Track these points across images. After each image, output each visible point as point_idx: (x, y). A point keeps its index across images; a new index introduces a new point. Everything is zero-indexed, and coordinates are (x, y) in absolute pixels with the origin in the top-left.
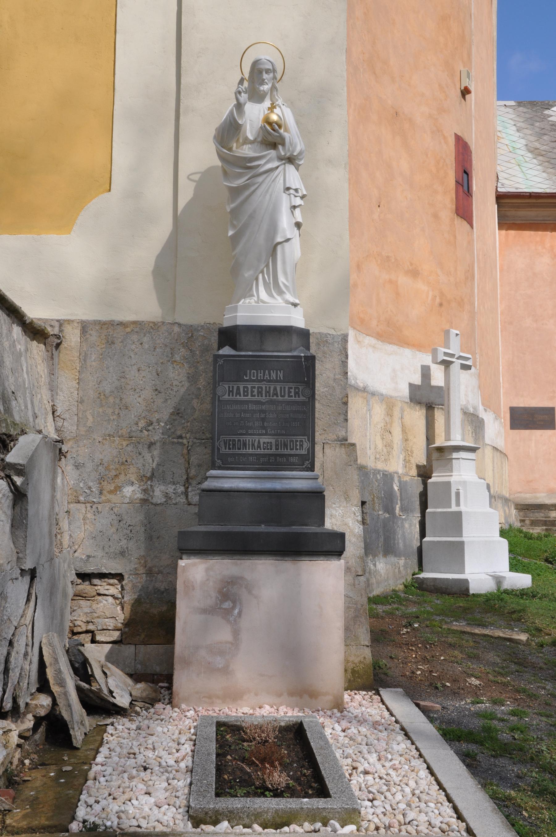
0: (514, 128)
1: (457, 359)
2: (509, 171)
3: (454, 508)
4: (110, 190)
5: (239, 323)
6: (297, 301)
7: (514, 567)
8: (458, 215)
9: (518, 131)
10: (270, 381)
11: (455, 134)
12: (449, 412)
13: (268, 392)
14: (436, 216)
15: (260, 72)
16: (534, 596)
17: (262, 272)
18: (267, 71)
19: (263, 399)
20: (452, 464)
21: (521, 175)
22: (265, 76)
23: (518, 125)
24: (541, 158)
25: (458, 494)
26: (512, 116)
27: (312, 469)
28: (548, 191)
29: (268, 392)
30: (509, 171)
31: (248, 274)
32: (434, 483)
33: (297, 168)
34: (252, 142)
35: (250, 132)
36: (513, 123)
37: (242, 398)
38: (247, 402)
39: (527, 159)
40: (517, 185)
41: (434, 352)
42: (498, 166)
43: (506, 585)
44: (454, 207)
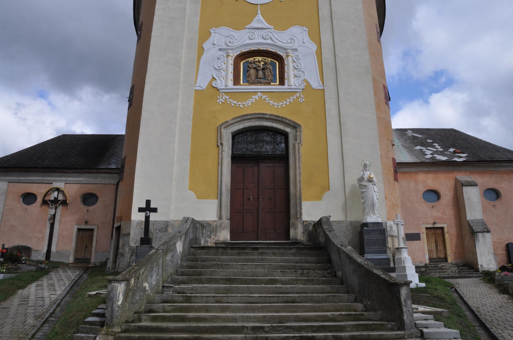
0: (397, 138)
1: (400, 222)
2: (398, 154)
3: (403, 265)
4: (329, 190)
5: (368, 222)
6: (379, 216)
7: (420, 281)
8: (395, 180)
9: (398, 139)
10: (376, 234)
11: (392, 158)
12: (399, 238)
13: (376, 237)
14: (389, 181)
15: (367, 166)
16: (427, 288)
17: (371, 210)
18: (368, 165)
19: (375, 238)
20: (401, 253)
21: (402, 156)
22: (368, 166)
23: (398, 137)
24: (407, 149)
25: (404, 261)
26: (395, 134)
27: (386, 253)
28: (412, 161)
29: (376, 237)
30: (398, 154)
31: (367, 210)
32: (397, 258)
33: (376, 186)
34: (366, 181)
35: (366, 179)
36: (396, 137)
37: (370, 238)
38: (371, 239)
39: (403, 150)
40: (401, 160)
41: (394, 221)
42: (396, 155)
43: (419, 286)
44: (394, 178)
